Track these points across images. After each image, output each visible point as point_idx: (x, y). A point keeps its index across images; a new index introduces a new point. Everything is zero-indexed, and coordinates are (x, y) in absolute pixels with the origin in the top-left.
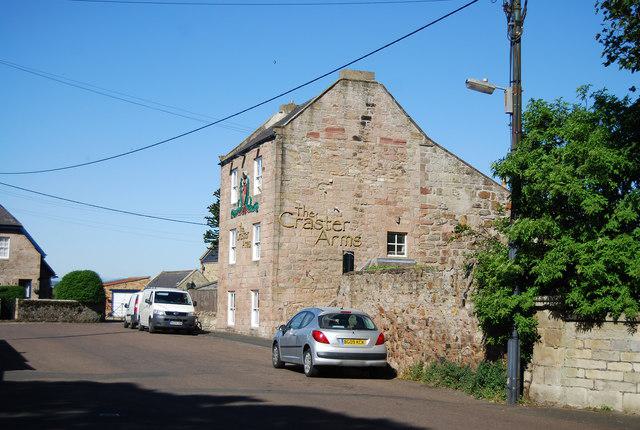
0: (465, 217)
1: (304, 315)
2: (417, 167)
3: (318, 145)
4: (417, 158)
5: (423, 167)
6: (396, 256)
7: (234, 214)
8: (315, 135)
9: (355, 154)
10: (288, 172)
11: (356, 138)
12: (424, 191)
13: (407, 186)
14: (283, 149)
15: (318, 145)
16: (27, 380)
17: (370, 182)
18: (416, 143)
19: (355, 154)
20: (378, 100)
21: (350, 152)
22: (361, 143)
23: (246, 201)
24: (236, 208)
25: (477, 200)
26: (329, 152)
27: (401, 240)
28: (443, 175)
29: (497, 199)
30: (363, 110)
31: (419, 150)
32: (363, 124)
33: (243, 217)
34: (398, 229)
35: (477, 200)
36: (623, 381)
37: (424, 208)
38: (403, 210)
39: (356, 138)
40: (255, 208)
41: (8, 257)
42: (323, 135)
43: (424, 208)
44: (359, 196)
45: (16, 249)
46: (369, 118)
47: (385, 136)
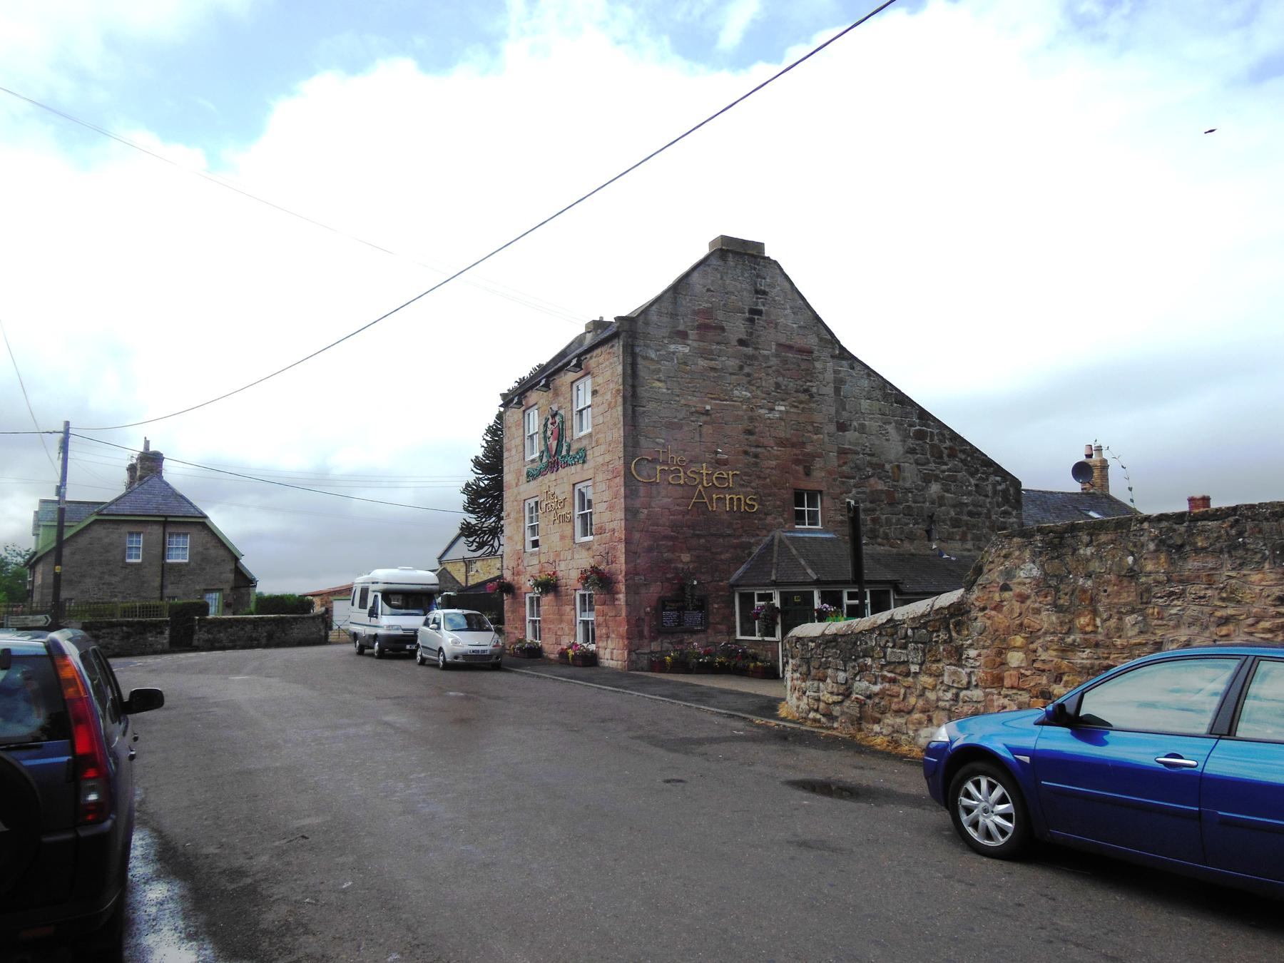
0: (898, 467)
1: (1010, 724)
2: (829, 390)
3: (687, 350)
4: (829, 376)
5: (837, 390)
6: (807, 526)
7: (531, 476)
8: (683, 335)
9: (741, 368)
10: (642, 392)
11: (742, 342)
12: (842, 427)
13: (818, 418)
14: (634, 356)
15: (687, 350)
16: (217, 652)
17: (762, 411)
18: (826, 354)
19: (741, 368)
20: (772, 286)
21: (732, 363)
22: (749, 351)
23: (558, 451)
24: (537, 465)
25: (911, 443)
26: (702, 363)
27: (812, 503)
28: (865, 404)
29: (936, 441)
30: (747, 300)
31: (830, 364)
32: (751, 321)
33: (551, 477)
34: (812, 485)
35: (911, 443)
36: (575, 590)
37: (842, 452)
38: (813, 456)
39: (742, 342)
40: (582, 457)
41: (187, 561)
42: (693, 334)
43: (842, 452)
44: (750, 432)
45: (200, 549)
46: (759, 313)
47: (783, 340)
